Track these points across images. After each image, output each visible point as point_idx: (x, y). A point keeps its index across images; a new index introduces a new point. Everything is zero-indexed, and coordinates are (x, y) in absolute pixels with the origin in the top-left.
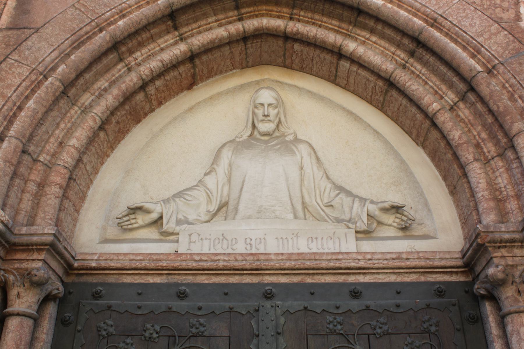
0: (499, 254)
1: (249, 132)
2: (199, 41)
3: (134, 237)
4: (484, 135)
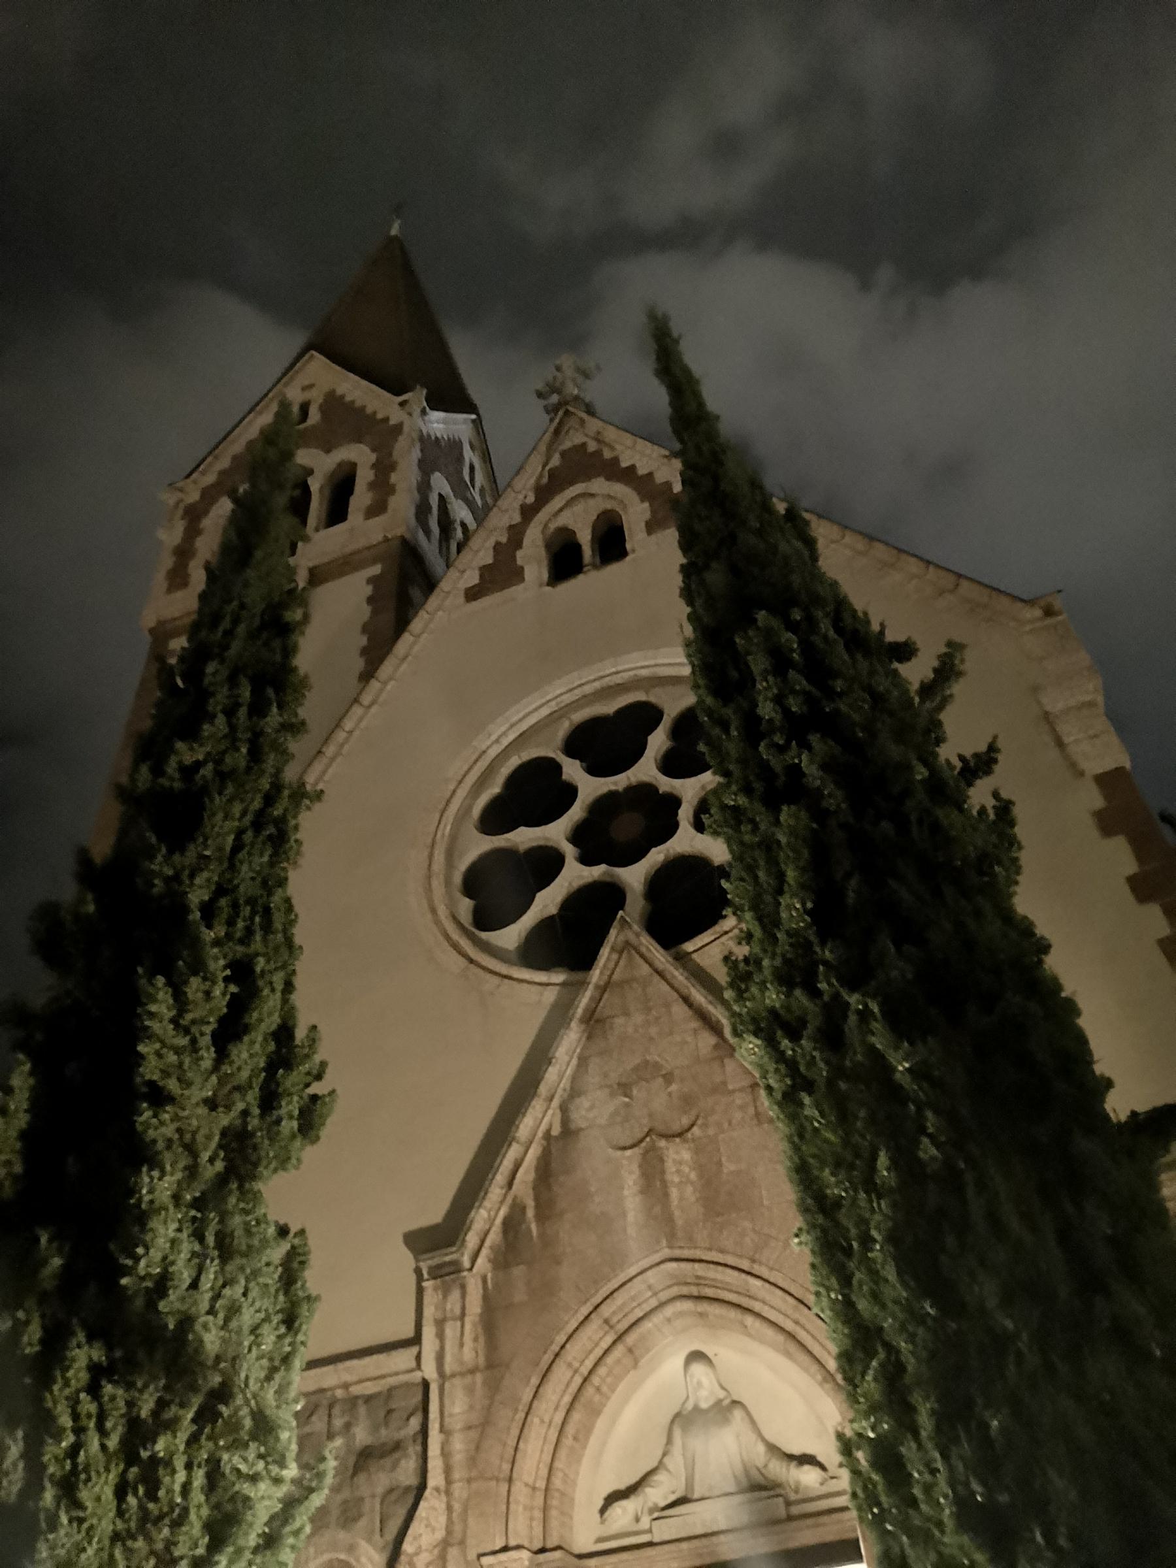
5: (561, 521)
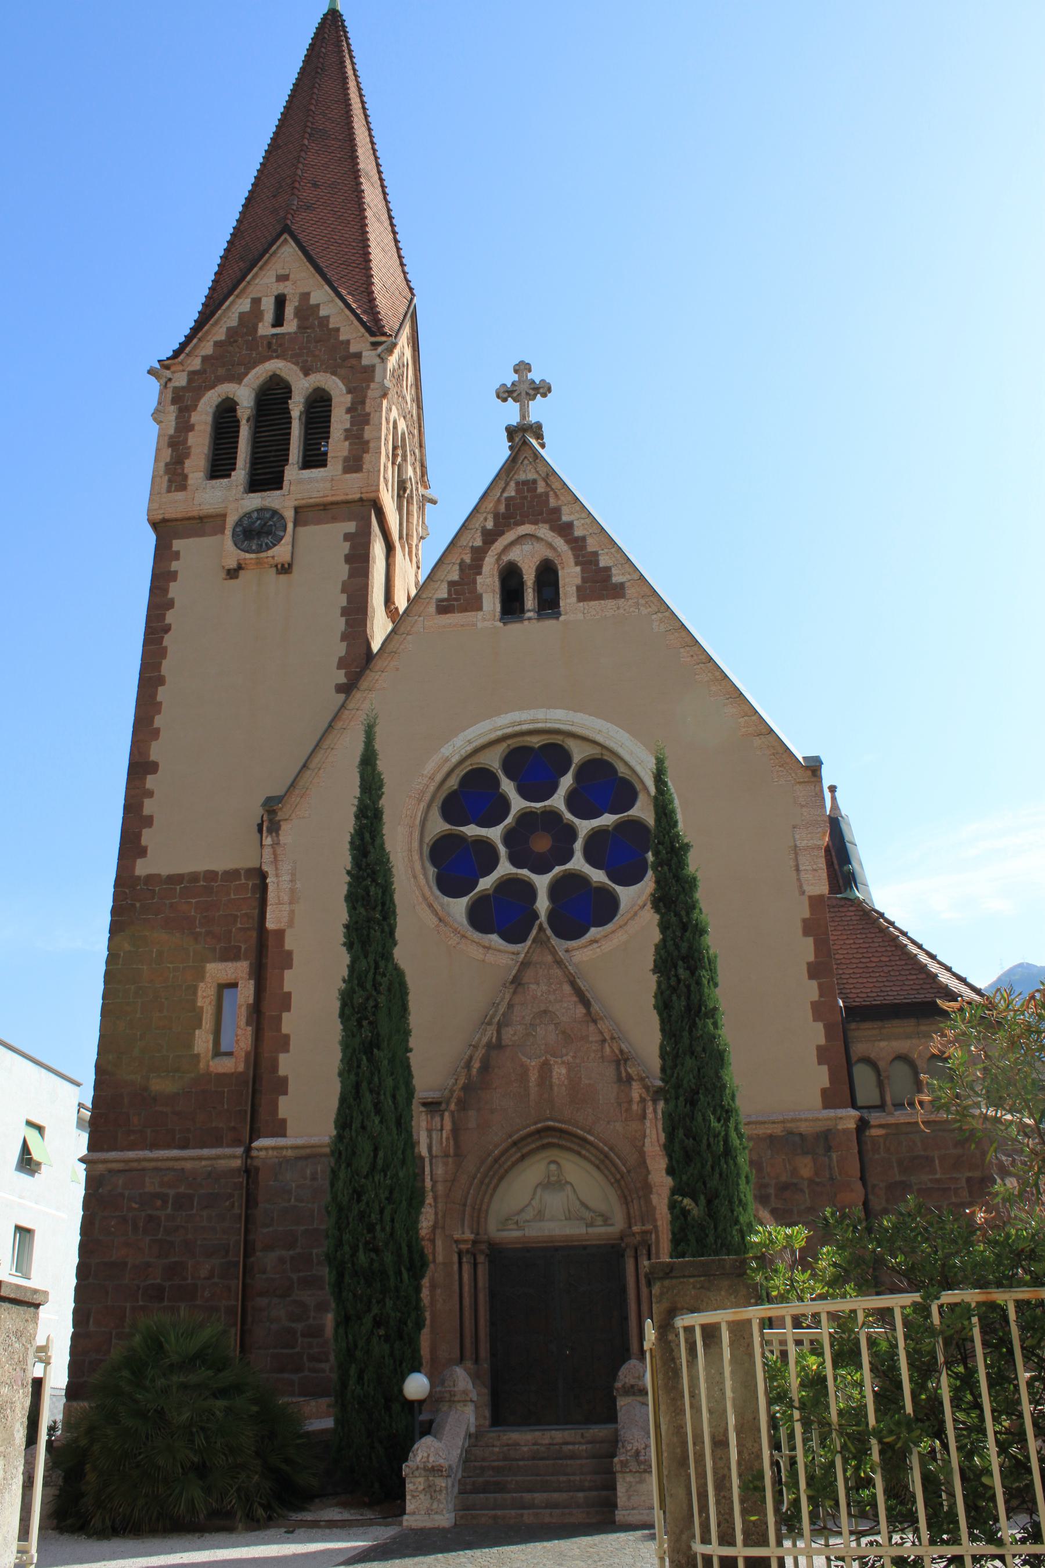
5: (506, 559)
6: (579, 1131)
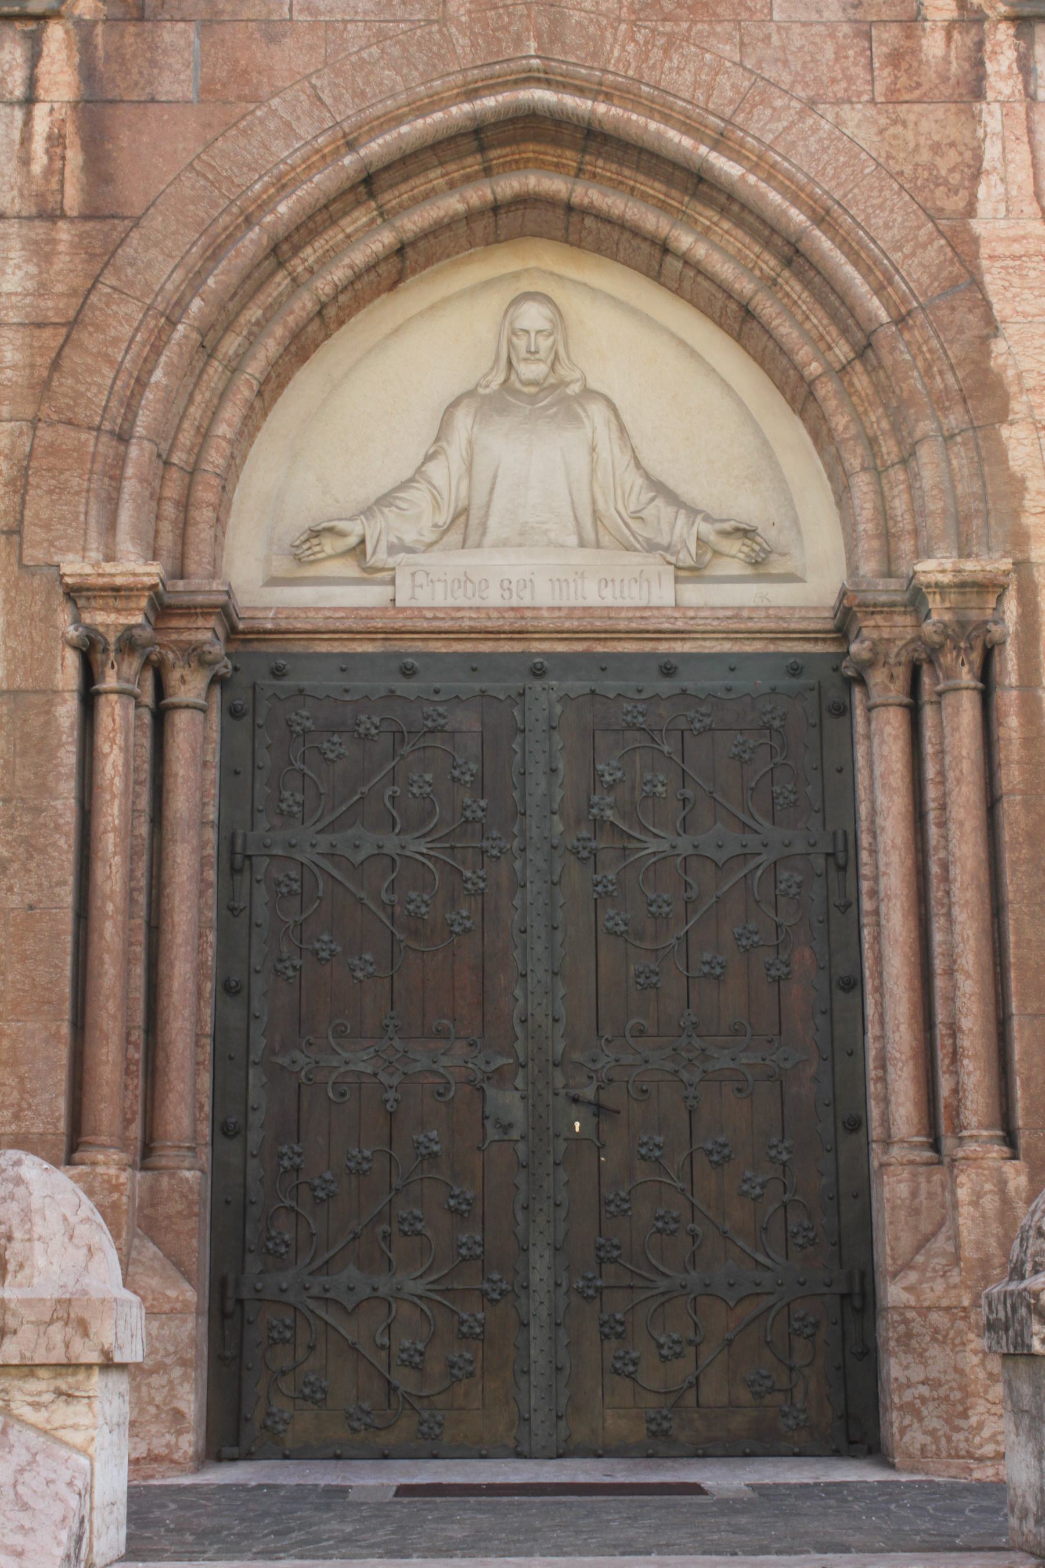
0: (871, 623)
1: (502, 378)
2: (414, 223)
3: (318, 574)
4: (885, 425)
6: (673, 135)
